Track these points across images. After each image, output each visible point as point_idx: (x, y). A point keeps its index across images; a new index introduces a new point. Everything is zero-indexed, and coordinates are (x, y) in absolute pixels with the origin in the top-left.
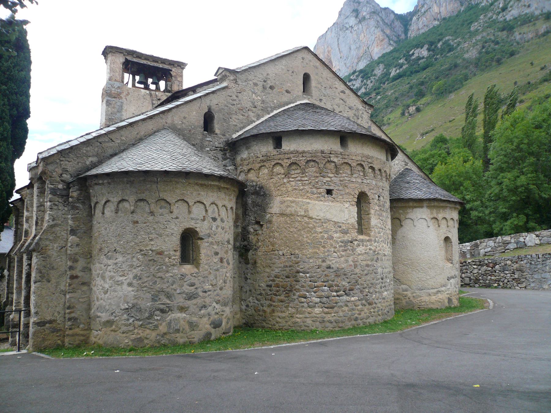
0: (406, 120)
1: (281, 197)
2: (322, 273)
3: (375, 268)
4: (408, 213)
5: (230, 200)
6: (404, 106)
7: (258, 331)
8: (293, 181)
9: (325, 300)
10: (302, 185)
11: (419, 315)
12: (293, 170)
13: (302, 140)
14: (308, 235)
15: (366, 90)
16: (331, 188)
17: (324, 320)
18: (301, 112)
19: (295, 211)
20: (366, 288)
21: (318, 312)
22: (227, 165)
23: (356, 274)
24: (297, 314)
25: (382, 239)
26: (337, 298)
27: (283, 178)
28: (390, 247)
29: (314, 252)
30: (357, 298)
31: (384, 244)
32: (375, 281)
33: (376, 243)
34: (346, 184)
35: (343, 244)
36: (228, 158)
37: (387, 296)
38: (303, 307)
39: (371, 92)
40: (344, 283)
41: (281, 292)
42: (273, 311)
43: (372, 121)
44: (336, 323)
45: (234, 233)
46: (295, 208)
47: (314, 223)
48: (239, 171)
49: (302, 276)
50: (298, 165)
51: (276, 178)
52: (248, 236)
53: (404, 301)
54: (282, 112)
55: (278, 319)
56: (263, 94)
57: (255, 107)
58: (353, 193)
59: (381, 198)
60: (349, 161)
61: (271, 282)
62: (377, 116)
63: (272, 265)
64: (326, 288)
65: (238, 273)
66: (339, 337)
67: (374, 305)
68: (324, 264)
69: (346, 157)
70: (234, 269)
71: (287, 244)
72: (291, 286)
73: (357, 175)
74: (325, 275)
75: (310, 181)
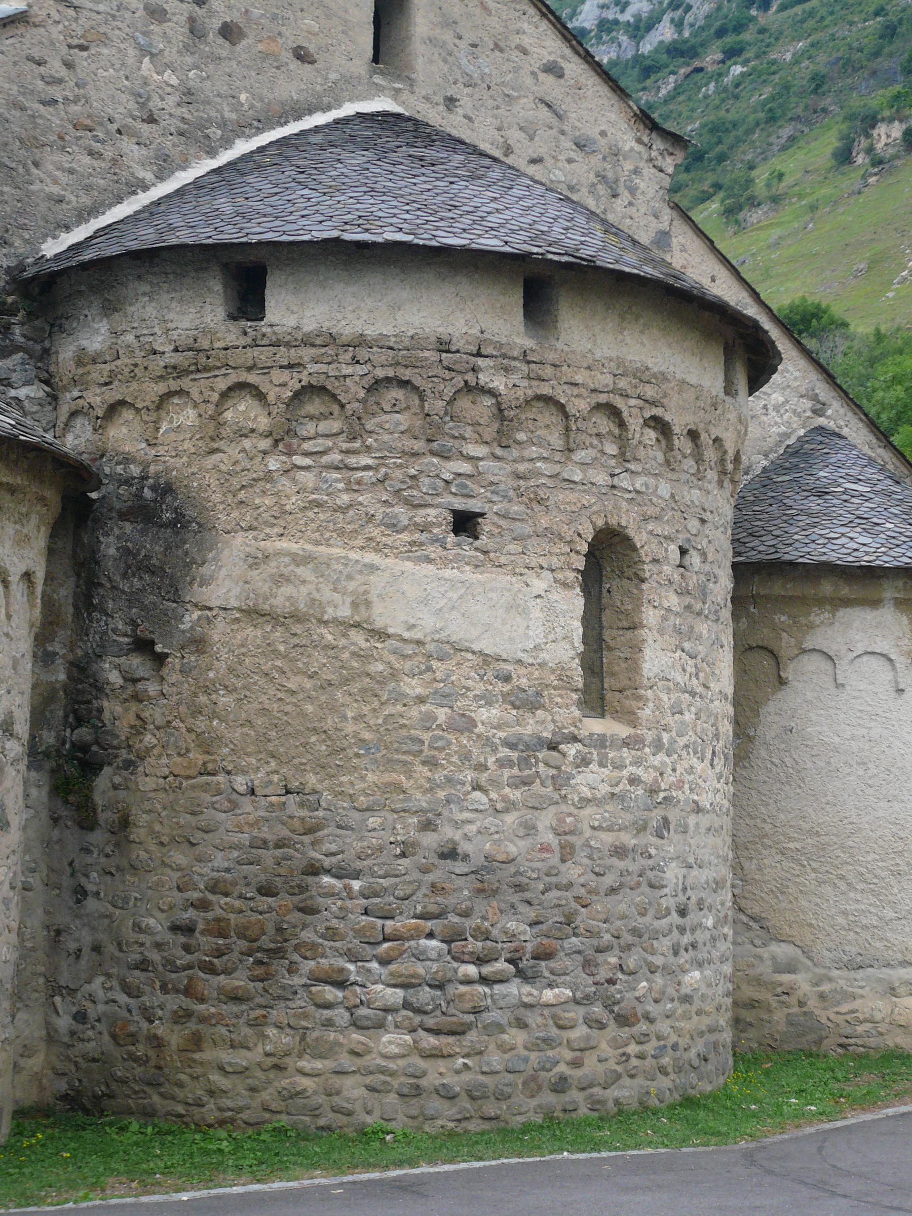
0: (858, 185)
1: (251, 534)
2: (416, 875)
3: (651, 862)
4: (811, 626)
5: (22, 541)
6: (850, 118)
7: (123, 1129)
8: (307, 468)
9: (425, 995)
10: (348, 490)
11: (839, 1075)
12: (311, 418)
13: (353, 289)
14: (366, 709)
15: (680, 33)
16: (474, 505)
17: (418, 1087)
18: (359, 158)
19: (313, 600)
20: (608, 949)
21: (396, 1050)
22: (15, 377)
23: (569, 886)
24: (300, 1056)
25: (690, 737)
26: (481, 989)
27: (265, 453)
28: (726, 772)
29: (387, 785)
30: (569, 993)
31: (695, 761)
32: (648, 919)
33: (661, 757)
34: (542, 493)
35: (515, 755)
36: (17, 349)
37: (704, 990)
38: (328, 1023)
39: (703, 45)
40: (512, 925)
41: (235, 956)
42: (196, 1041)
43: (676, 207)
44: (473, 1098)
45: (34, 687)
46: (311, 587)
47: (392, 658)
48: (64, 411)
49: (333, 886)
50: (334, 397)
51: (233, 451)
52: (96, 704)
53: (779, 1016)
54: (273, 151)
55: (215, 1077)
56: (189, 59)
57: (151, 120)
58: (569, 534)
59: (694, 559)
60: (559, 390)
61: (191, 913)
62: (721, 158)
63: (199, 835)
64: (434, 943)
65: (43, 867)
66: (481, 1159)
67: (643, 1027)
68: (429, 840)
69: (549, 371)
70: (27, 850)
71: (270, 747)
72: (280, 930)
73: (591, 453)
74: (433, 885)
75: (383, 470)
